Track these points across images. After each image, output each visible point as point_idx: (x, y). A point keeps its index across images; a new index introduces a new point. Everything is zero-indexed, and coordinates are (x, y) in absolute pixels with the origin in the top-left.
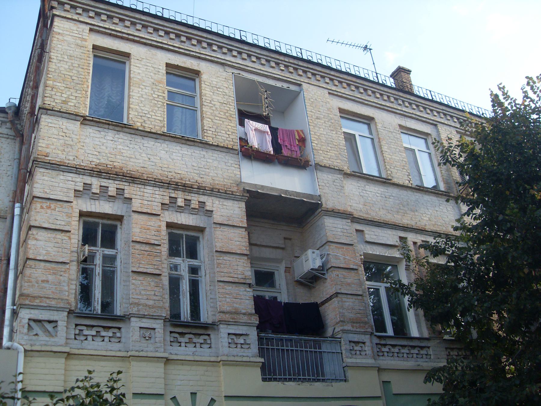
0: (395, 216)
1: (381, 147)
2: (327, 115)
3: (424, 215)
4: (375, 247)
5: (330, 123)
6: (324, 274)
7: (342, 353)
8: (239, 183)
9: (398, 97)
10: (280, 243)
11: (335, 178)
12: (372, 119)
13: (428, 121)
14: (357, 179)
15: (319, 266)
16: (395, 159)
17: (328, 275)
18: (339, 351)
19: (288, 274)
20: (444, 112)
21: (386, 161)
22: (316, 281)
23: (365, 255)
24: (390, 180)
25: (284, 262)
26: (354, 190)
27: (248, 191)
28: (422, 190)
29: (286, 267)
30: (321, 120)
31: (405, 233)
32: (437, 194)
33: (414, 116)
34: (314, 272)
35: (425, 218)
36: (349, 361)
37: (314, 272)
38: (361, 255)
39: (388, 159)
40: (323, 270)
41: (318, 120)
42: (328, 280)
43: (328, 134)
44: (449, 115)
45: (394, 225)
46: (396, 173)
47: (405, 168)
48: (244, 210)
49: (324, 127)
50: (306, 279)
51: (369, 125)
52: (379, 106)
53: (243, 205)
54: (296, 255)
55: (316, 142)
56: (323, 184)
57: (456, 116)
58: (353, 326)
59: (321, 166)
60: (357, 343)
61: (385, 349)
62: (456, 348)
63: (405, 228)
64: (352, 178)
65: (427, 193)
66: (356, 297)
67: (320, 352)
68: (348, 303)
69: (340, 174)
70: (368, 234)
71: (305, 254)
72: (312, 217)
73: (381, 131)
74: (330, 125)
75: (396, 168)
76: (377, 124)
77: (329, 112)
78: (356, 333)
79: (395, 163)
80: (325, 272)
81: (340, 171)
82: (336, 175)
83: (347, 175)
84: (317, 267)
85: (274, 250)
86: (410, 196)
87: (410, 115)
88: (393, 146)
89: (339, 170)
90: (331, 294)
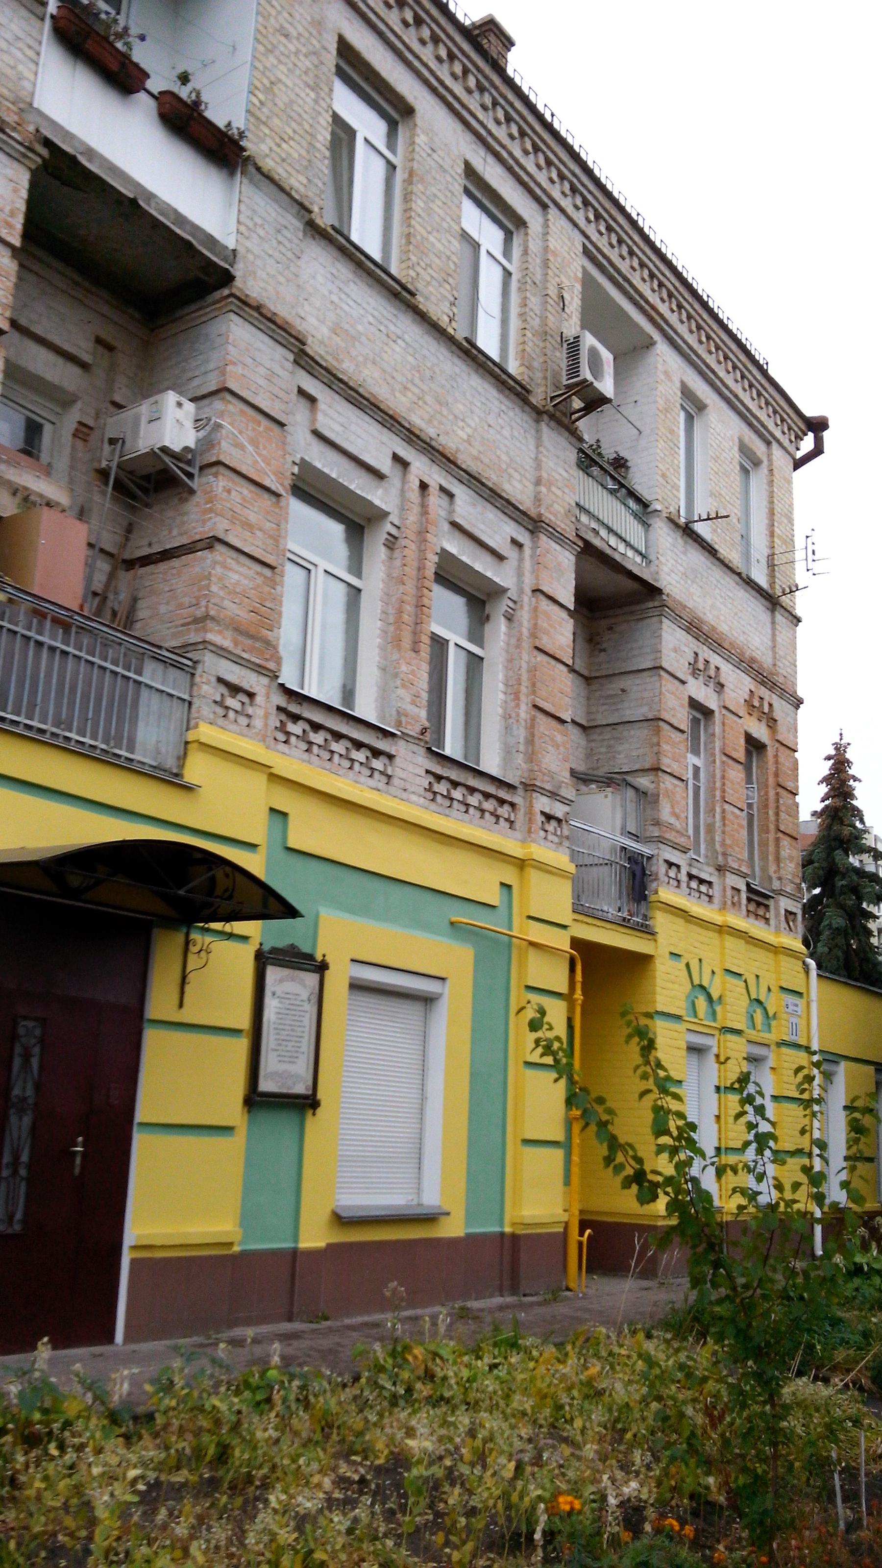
0: (397, 394)
1: (407, 197)
2: (307, 35)
3: (461, 424)
4: (333, 456)
5: (308, 63)
6: (190, 476)
7: (190, 703)
8: (27, 107)
9: (487, 85)
10: (83, 348)
11: (284, 223)
12: (408, 111)
13: (532, 185)
14: (335, 253)
15: (186, 449)
16: (433, 245)
17: (204, 480)
18: (186, 697)
19: (80, 444)
20: (575, 181)
21: (412, 240)
22: (156, 490)
23: (304, 465)
24: (412, 294)
25: (79, 405)
26: (320, 279)
27: (47, 143)
28: (474, 359)
29: (80, 423)
30: (290, 42)
31: (410, 448)
32: (503, 383)
33: (505, 155)
34: (167, 459)
35: (460, 433)
36: (206, 732)
37: (167, 459)
38: (294, 463)
39: (419, 237)
40: (189, 463)
41: (283, 39)
42: (198, 498)
43: (297, 90)
44: (582, 194)
45: (391, 417)
46: (428, 283)
47: (451, 280)
48: (24, 194)
49: (291, 66)
50: (131, 473)
51: (393, 126)
52: (435, 83)
53: (24, 178)
54: (118, 398)
55: (261, 96)
56: (250, 224)
57: (597, 205)
58: (236, 644)
59: (258, 169)
60: (235, 690)
61: (296, 728)
62: (448, 779)
63: (412, 436)
64: (323, 243)
65: (481, 371)
66: (258, 568)
67: (139, 683)
68: (236, 577)
69: (298, 216)
70: (326, 415)
71: (152, 399)
72: (193, 307)
73: (422, 153)
74: (308, 69)
75: (430, 271)
76: (418, 131)
77: (314, 32)
78: (238, 661)
79: (431, 256)
80: (195, 471)
81: (302, 208)
82: (290, 217)
83: (313, 229)
84: (177, 447)
85: (60, 361)
86: (441, 358)
87: (498, 148)
88: (437, 209)
89: (301, 205)
90: (198, 537)
